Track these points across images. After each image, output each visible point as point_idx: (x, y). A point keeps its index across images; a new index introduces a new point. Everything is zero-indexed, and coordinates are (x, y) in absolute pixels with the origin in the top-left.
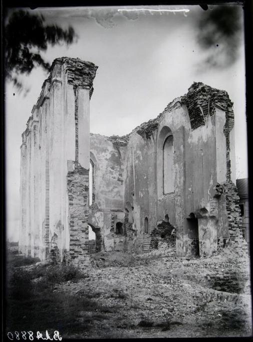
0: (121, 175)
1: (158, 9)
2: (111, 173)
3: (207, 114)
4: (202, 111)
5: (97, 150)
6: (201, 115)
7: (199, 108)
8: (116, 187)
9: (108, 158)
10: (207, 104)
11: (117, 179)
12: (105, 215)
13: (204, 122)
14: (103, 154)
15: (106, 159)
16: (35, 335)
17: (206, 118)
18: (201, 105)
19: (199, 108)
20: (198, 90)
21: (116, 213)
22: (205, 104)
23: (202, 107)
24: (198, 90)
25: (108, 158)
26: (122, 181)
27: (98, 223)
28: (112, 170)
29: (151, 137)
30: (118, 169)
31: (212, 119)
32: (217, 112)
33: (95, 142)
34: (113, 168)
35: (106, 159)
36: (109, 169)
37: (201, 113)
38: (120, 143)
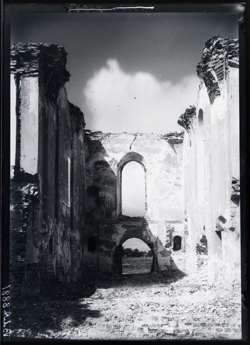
0: (178, 178)
1: (98, 9)
2: (167, 177)
3: (222, 79)
4: (215, 76)
5: (148, 152)
6: (214, 82)
7: (209, 72)
8: (173, 194)
9: (162, 160)
10: (222, 64)
11: (173, 184)
12: (159, 227)
13: (219, 92)
14: (156, 155)
15: (160, 162)
16: (7, 309)
17: (220, 85)
18: (214, 67)
19: (209, 72)
20: (211, 47)
21: (172, 225)
22: (218, 66)
23: (215, 70)
24: (211, 47)
25: (162, 160)
26: (180, 186)
27: (150, 238)
28: (167, 174)
29: (190, 126)
30: (175, 172)
31: (227, 82)
32: (231, 72)
33: (146, 143)
34: (168, 171)
35: (160, 162)
36: (164, 172)
37: (214, 79)
38: (174, 139)
